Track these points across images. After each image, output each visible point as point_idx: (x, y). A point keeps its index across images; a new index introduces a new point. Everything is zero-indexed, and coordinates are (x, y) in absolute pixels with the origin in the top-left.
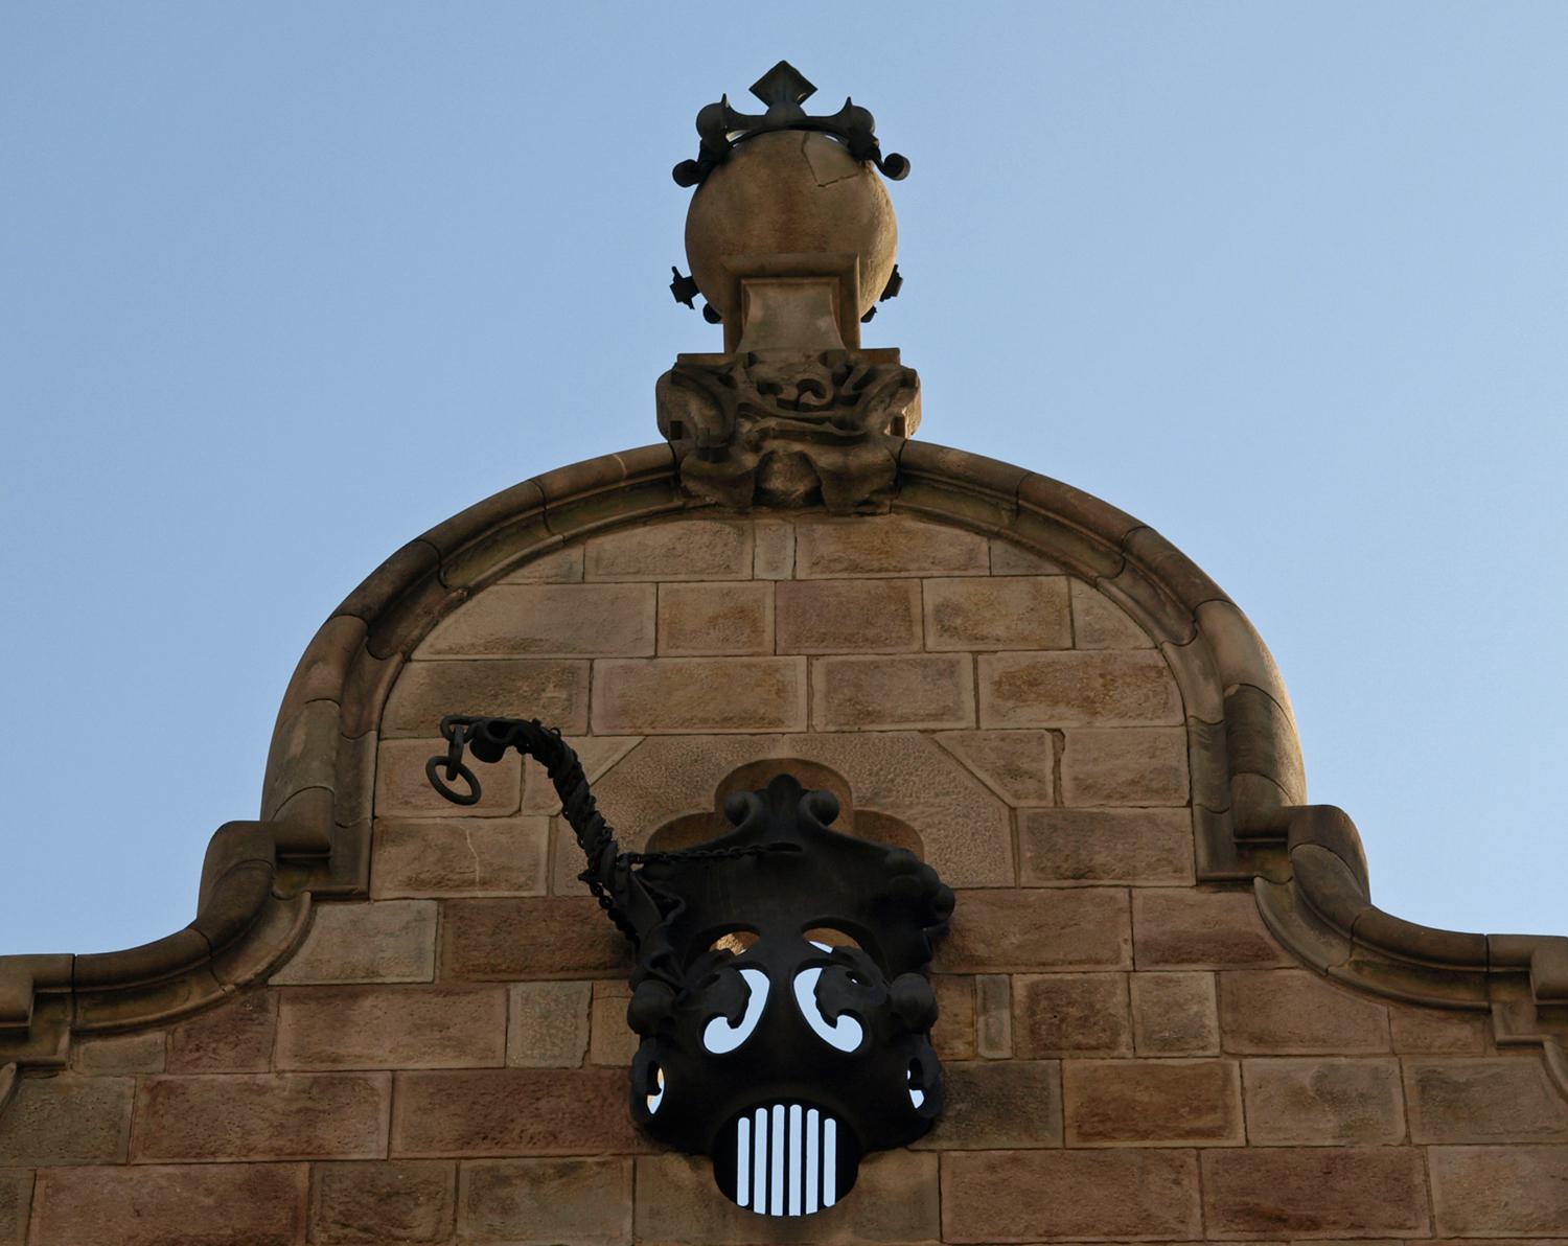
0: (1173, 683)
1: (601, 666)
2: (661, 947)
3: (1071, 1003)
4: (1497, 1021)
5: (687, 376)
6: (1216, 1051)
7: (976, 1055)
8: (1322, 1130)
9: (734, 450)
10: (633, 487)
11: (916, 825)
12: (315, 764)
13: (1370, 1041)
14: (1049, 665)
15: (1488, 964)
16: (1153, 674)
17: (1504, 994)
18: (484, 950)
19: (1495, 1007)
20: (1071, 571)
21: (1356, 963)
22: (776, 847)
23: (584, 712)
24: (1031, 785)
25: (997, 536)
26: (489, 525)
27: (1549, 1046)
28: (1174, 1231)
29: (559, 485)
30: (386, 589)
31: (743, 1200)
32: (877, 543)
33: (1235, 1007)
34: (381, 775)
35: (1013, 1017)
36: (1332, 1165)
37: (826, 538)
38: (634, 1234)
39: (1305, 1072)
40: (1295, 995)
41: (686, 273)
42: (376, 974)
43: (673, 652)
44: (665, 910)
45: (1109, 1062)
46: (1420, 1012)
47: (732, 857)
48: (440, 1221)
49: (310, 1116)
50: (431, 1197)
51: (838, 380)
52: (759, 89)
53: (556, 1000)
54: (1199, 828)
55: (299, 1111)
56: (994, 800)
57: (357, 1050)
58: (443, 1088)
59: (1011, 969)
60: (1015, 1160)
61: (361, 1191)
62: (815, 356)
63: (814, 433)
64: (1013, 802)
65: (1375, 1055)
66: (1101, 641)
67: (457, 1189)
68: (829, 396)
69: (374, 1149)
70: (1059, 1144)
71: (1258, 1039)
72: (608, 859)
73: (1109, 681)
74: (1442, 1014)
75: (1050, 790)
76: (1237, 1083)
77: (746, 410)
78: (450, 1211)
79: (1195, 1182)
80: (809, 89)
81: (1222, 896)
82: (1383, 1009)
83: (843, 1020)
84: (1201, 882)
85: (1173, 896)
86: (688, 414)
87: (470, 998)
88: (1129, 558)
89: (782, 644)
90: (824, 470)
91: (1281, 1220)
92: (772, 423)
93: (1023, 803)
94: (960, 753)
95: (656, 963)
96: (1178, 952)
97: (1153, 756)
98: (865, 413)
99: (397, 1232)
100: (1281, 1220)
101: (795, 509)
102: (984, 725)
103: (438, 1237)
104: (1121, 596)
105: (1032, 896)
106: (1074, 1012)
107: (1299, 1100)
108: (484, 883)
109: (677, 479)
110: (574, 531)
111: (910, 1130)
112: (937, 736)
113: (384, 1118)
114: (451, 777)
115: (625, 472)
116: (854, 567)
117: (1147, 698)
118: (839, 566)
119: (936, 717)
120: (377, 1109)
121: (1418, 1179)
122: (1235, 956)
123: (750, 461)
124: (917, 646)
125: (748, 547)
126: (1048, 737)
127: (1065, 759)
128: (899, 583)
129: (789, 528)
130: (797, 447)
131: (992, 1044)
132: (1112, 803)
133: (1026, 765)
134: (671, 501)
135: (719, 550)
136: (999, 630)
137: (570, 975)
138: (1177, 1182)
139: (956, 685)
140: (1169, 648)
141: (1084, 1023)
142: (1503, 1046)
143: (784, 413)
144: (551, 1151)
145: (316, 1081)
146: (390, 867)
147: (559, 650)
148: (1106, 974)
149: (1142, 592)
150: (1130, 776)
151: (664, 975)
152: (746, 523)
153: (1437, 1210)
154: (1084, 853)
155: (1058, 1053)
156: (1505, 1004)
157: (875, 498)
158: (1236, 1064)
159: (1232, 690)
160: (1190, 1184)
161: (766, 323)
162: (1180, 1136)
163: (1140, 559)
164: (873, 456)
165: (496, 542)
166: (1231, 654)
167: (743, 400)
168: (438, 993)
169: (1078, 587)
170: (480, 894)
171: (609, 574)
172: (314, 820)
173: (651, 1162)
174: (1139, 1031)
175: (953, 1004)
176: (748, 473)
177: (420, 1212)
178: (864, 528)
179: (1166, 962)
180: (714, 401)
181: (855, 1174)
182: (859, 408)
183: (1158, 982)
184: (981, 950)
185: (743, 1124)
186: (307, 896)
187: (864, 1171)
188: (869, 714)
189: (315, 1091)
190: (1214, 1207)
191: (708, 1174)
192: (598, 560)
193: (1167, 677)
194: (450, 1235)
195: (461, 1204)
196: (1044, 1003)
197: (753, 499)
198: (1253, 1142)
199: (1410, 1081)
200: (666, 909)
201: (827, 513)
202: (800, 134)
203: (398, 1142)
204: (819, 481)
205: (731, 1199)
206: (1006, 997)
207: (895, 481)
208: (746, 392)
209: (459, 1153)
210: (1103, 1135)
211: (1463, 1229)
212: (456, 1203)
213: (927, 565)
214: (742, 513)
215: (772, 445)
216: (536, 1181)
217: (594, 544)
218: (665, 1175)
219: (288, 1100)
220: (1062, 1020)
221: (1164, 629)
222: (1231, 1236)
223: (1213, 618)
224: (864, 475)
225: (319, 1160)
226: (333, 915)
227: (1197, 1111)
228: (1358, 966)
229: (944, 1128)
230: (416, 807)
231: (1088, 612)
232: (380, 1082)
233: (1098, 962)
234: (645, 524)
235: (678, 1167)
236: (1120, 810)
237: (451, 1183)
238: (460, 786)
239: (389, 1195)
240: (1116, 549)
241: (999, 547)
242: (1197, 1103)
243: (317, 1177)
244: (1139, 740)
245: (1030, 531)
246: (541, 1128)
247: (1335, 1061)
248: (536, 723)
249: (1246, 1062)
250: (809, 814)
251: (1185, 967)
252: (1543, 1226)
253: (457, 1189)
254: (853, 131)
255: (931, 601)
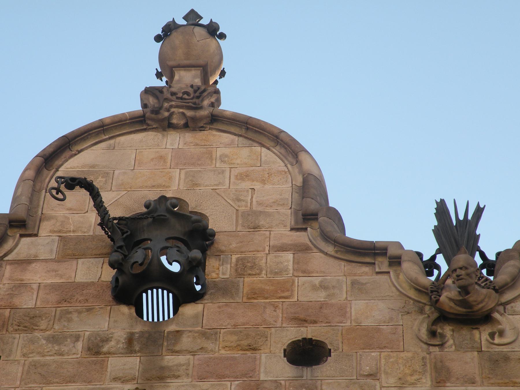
0: (289, 176)
1: (117, 172)
2: (121, 243)
3: (248, 262)
4: (377, 266)
5: (149, 91)
6: (291, 275)
7: (219, 277)
8: (321, 296)
9: (162, 111)
10: (131, 123)
11: (207, 215)
12: (24, 197)
13: (336, 272)
14: (252, 171)
15: (374, 250)
16: (284, 173)
17: (380, 259)
18: (71, 249)
19: (376, 262)
20: (262, 145)
21: (336, 251)
22: (159, 216)
23: (110, 184)
24: (243, 203)
25: (240, 136)
26: (85, 132)
27: (392, 274)
28: (273, 324)
29: (108, 121)
30: (51, 150)
31: (145, 318)
32: (204, 138)
33: (298, 263)
34: (46, 202)
35: (231, 267)
36: (322, 306)
37: (189, 137)
38: (108, 327)
39: (317, 281)
40: (317, 260)
41: (160, 70)
42: (37, 256)
43: (139, 168)
44: (123, 234)
45: (259, 278)
46: (354, 264)
47: (145, 218)
48: (49, 324)
49: (11, 296)
50: (46, 318)
51: (195, 92)
52: (185, 18)
53: (92, 263)
54: (293, 214)
55: (8, 294)
56: (232, 208)
57: (28, 278)
58: (53, 288)
59: (231, 254)
60: (226, 305)
61: (25, 316)
62: (189, 85)
63: (186, 106)
64: (237, 208)
65: (339, 276)
66: (268, 164)
67: (55, 316)
68: (192, 96)
69: (31, 305)
70: (240, 301)
71: (304, 272)
72: (106, 218)
73: (270, 175)
74: (360, 265)
75: (249, 205)
76: (297, 284)
77: (167, 100)
78: (52, 322)
79: (281, 311)
80: (201, 18)
81: (298, 233)
82: (343, 263)
83: (174, 263)
84: (292, 229)
85: (282, 232)
86: (149, 101)
87: (66, 263)
88: (279, 141)
89: (172, 166)
90: (190, 117)
91: (305, 321)
92: (173, 103)
93: (240, 209)
94: (223, 195)
95: (118, 248)
96: (283, 248)
97: (281, 195)
98: (203, 100)
99: (35, 327)
100: (305, 321)
101: (180, 129)
102: (231, 187)
103: (47, 329)
104: (276, 152)
105: (240, 233)
106: (249, 264)
107: (314, 288)
108: (74, 231)
109: (145, 120)
110: (112, 135)
111: (196, 297)
112: (217, 191)
113: (35, 297)
114: (57, 193)
115: (129, 118)
116: (197, 145)
117: (281, 179)
118: (192, 144)
119: (217, 185)
120: (33, 293)
121: (348, 310)
122: (300, 249)
123: (166, 114)
124: (213, 166)
125: (165, 140)
126: (250, 190)
127: (254, 196)
128: (210, 149)
129: (178, 134)
130: (181, 110)
131: (223, 274)
132: (267, 208)
133: (242, 198)
134: (143, 126)
135: (156, 140)
136: (238, 161)
137: (97, 256)
138: (275, 311)
139: (224, 176)
140: (289, 166)
141: (252, 268)
142: (378, 273)
143: (178, 100)
144: (85, 305)
145: (14, 286)
146: (45, 229)
147: (104, 168)
148: (259, 255)
149: (283, 151)
150: (273, 201)
151: (121, 251)
152: (165, 133)
153: (353, 318)
154: (257, 221)
155: (243, 276)
156: (379, 261)
157: (204, 126)
158: (297, 279)
159: (305, 176)
160: (279, 312)
161: (179, 81)
162: (278, 298)
163: (282, 141)
164: (204, 113)
165: (88, 138)
166: (307, 165)
167: (165, 97)
168: (56, 262)
169: (264, 149)
170: (72, 235)
171: (122, 147)
172: (22, 213)
173: (116, 307)
174: (269, 270)
175: (211, 264)
176: (165, 118)
177: (43, 322)
178: (201, 134)
179: (279, 251)
180: (157, 98)
181: (178, 310)
182: (201, 99)
183: (275, 257)
184: (223, 248)
185: (144, 295)
186: (18, 235)
187: (181, 309)
188: (196, 184)
189: (14, 289)
190: (286, 318)
191: (133, 310)
192: (119, 143)
193: (288, 174)
194: (52, 328)
195: (56, 320)
196: (240, 262)
197: (167, 126)
198: (300, 300)
199: (349, 283)
200: (125, 236)
201: (190, 130)
202: (193, 26)
203: (38, 303)
204: (187, 120)
205: (140, 317)
206: (230, 261)
207: (211, 120)
208: (167, 95)
209: (57, 306)
210: (254, 298)
211: (361, 323)
212: (54, 319)
213: (219, 144)
214: (164, 130)
215: (173, 110)
216: (80, 312)
217: (118, 139)
218: (120, 311)
219: (5, 291)
220: (245, 267)
221: (288, 161)
222: (290, 326)
223: (302, 156)
224: (201, 119)
225: (13, 308)
226: (25, 241)
227: (283, 291)
228: (337, 252)
229: (206, 297)
230: (55, 211)
231: (266, 156)
232: (35, 286)
233: (258, 251)
234: (134, 133)
235: (125, 309)
236: (269, 210)
237: (53, 314)
238: (60, 196)
239: (33, 317)
240: (275, 138)
241: (241, 139)
242: (283, 289)
243: (12, 312)
244: (277, 191)
245: (250, 135)
246: (83, 298)
247: (327, 278)
248: (85, 179)
249: (300, 278)
250: (169, 206)
251: (284, 252)
252: (384, 322)
253: (55, 316)
254: (213, 30)
255: (218, 154)
